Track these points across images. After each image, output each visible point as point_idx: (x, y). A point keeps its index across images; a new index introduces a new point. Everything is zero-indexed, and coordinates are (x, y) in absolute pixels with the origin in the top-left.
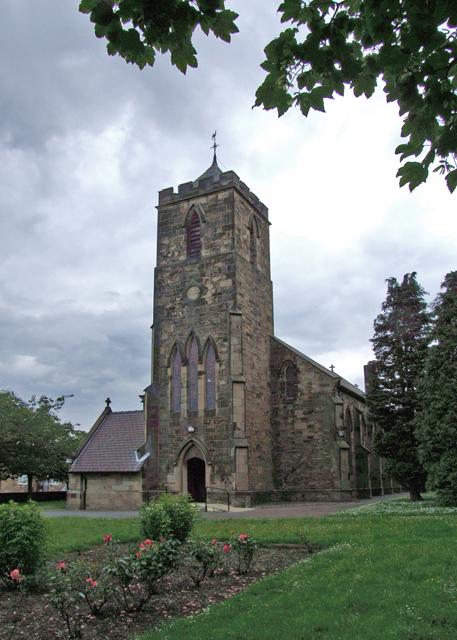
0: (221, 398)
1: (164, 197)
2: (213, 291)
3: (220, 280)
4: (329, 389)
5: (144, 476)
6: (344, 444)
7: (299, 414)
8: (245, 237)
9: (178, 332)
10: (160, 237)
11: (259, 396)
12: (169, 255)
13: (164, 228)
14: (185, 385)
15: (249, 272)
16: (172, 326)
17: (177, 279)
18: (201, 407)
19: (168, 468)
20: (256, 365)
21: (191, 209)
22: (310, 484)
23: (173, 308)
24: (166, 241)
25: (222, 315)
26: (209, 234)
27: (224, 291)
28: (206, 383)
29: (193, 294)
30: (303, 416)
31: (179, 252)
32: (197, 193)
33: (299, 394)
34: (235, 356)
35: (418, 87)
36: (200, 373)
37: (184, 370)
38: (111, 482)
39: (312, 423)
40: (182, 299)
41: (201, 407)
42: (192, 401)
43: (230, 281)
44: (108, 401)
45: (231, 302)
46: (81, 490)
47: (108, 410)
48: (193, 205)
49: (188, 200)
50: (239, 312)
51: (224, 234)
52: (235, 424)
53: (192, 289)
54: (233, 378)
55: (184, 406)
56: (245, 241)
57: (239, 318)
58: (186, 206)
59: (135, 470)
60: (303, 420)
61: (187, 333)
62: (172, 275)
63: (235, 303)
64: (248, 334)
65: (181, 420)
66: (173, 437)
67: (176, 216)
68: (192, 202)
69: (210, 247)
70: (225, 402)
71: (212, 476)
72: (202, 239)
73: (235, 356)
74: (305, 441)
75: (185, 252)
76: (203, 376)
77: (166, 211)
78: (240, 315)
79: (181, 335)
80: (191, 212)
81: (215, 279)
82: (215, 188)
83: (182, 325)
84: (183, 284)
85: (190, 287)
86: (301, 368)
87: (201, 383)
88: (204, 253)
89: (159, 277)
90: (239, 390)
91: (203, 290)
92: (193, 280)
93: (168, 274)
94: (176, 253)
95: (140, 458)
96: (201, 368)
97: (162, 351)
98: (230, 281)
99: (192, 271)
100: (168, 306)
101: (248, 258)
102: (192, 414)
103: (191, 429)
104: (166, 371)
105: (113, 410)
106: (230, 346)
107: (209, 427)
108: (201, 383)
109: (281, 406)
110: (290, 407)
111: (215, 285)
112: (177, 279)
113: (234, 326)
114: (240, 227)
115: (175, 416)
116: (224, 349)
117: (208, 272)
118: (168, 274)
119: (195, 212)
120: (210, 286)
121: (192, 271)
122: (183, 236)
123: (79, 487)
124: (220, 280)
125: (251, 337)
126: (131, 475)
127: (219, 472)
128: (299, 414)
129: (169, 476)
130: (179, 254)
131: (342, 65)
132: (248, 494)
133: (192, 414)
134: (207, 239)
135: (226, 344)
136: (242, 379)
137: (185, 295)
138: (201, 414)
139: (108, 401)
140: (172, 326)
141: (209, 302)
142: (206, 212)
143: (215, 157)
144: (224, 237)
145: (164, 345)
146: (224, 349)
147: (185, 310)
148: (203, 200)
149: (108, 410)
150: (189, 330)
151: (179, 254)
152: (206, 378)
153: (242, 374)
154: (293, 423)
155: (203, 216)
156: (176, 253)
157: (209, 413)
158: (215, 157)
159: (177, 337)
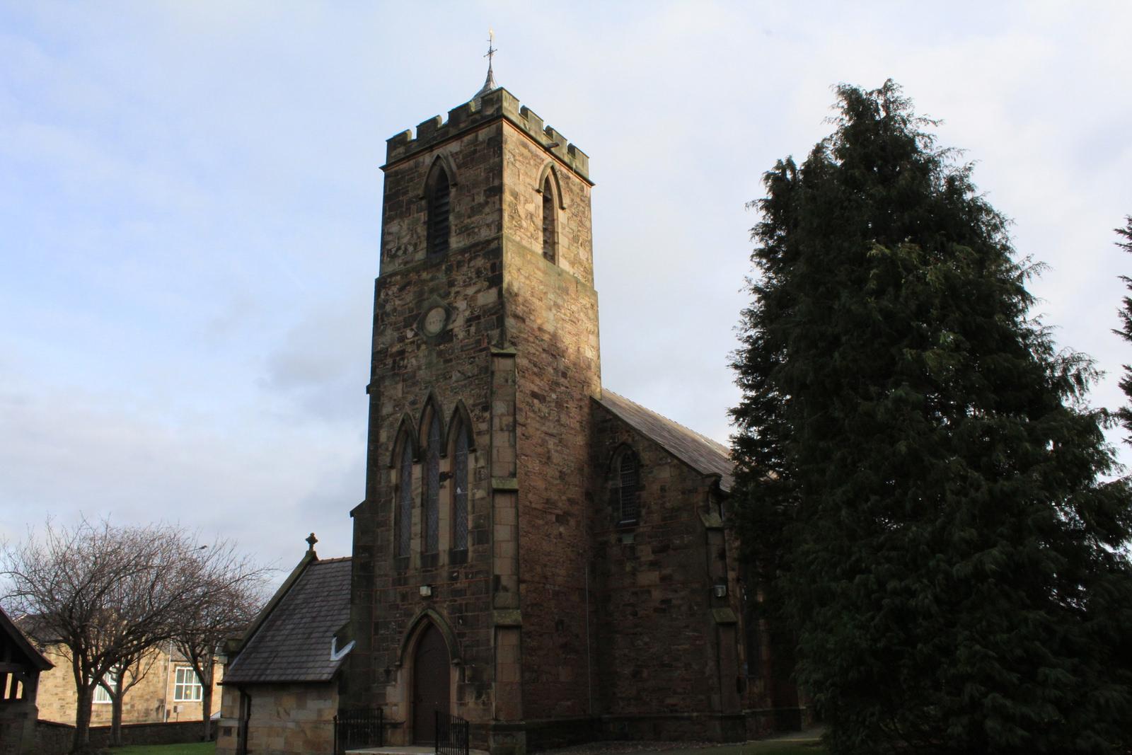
0: (477, 526)
1: (395, 148)
2: (467, 313)
3: (479, 291)
4: (698, 499)
5: (342, 692)
6: (728, 614)
7: (646, 553)
8: (531, 207)
9: (411, 398)
10: (387, 220)
11: (561, 519)
12: (400, 253)
13: (395, 203)
14: (418, 501)
15: (540, 275)
16: (400, 386)
17: (409, 297)
18: (444, 544)
19: (388, 672)
20: (555, 455)
21: (434, 164)
22: (669, 701)
23: (402, 353)
24: (394, 228)
25: (481, 359)
26: (462, 208)
27: (486, 311)
28: (455, 498)
29: (434, 323)
30: (652, 557)
31: (415, 245)
32: (447, 132)
33: (644, 512)
34: (501, 440)
35: (1095, 486)
36: (444, 476)
37: (417, 471)
38: (289, 701)
39: (668, 571)
40: (416, 335)
41: (444, 544)
42: (429, 536)
43: (494, 291)
44: (312, 540)
45: (495, 333)
46: (240, 719)
47: (311, 556)
48: (438, 157)
49: (431, 149)
50: (511, 350)
51: (487, 203)
52: (497, 578)
53: (433, 313)
54: (495, 484)
55: (416, 545)
56: (531, 216)
57: (509, 362)
58: (427, 159)
59: (325, 677)
60: (654, 565)
61: (425, 398)
62: (402, 289)
63: (503, 333)
64: (534, 395)
65: (411, 572)
66: (397, 607)
67: (412, 180)
68: (436, 153)
69: (466, 230)
70: (483, 534)
71: (461, 690)
72: (451, 218)
73: (501, 440)
74: (656, 610)
75: (424, 245)
76: (447, 483)
77: (396, 173)
78: (512, 356)
79: (413, 403)
80: (436, 171)
81: (470, 291)
82: (474, 121)
83: (414, 384)
84: (420, 302)
85: (430, 309)
86: (646, 457)
87: (444, 498)
88: (455, 242)
89: (382, 296)
90: (505, 508)
91: (449, 312)
92: (435, 296)
93: (395, 289)
94: (411, 249)
95: (337, 651)
96: (444, 466)
97: (383, 436)
98: (494, 291)
99: (432, 279)
100: (395, 349)
101: (538, 247)
102: (429, 559)
103: (425, 591)
104: (389, 475)
105: (320, 557)
106: (491, 419)
107: (458, 586)
108: (444, 498)
109: (613, 538)
110: (628, 540)
111: (471, 300)
112: (409, 297)
113: (498, 380)
114: (520, 189)
115: (402, 563)
116: (483, 426)
117: (460, 279)
118: (395, 289)
119: (442, 170)
120: (461, 305)
121: (432, 279)
122: (423, 216)
123: (237, 714)
124: (479, 291)
125: (542, 399)
126: (318, 687)
127: (472, 679)
128: (646, 553)
129: (389, 690)
130: (415, 250)
131: (878, 169)
132: (519, 728)
133: (429, 559)
134: (459, 216)
135: (487, 415)
136: (514, 484)
137: (422, 326)
138: (444, 559)
139: (312, 540)
140: (400, 386)
141: (461, 336)
142: (459, 167)
143: (490, 72)
144: (487, 210)
145: (386, 423)
146: (483, 426)
147: (421, 354)
148: (454, 147)
149: (311, 556)
150: (427, 392)
151: (415, 250)
152: (454, 487)
153: (513, 475)
154: (634, 573)
155: (453, 174)
156: (411, 249)
157: (457, 557)
158: (490, 72)
159: (408, 409)
